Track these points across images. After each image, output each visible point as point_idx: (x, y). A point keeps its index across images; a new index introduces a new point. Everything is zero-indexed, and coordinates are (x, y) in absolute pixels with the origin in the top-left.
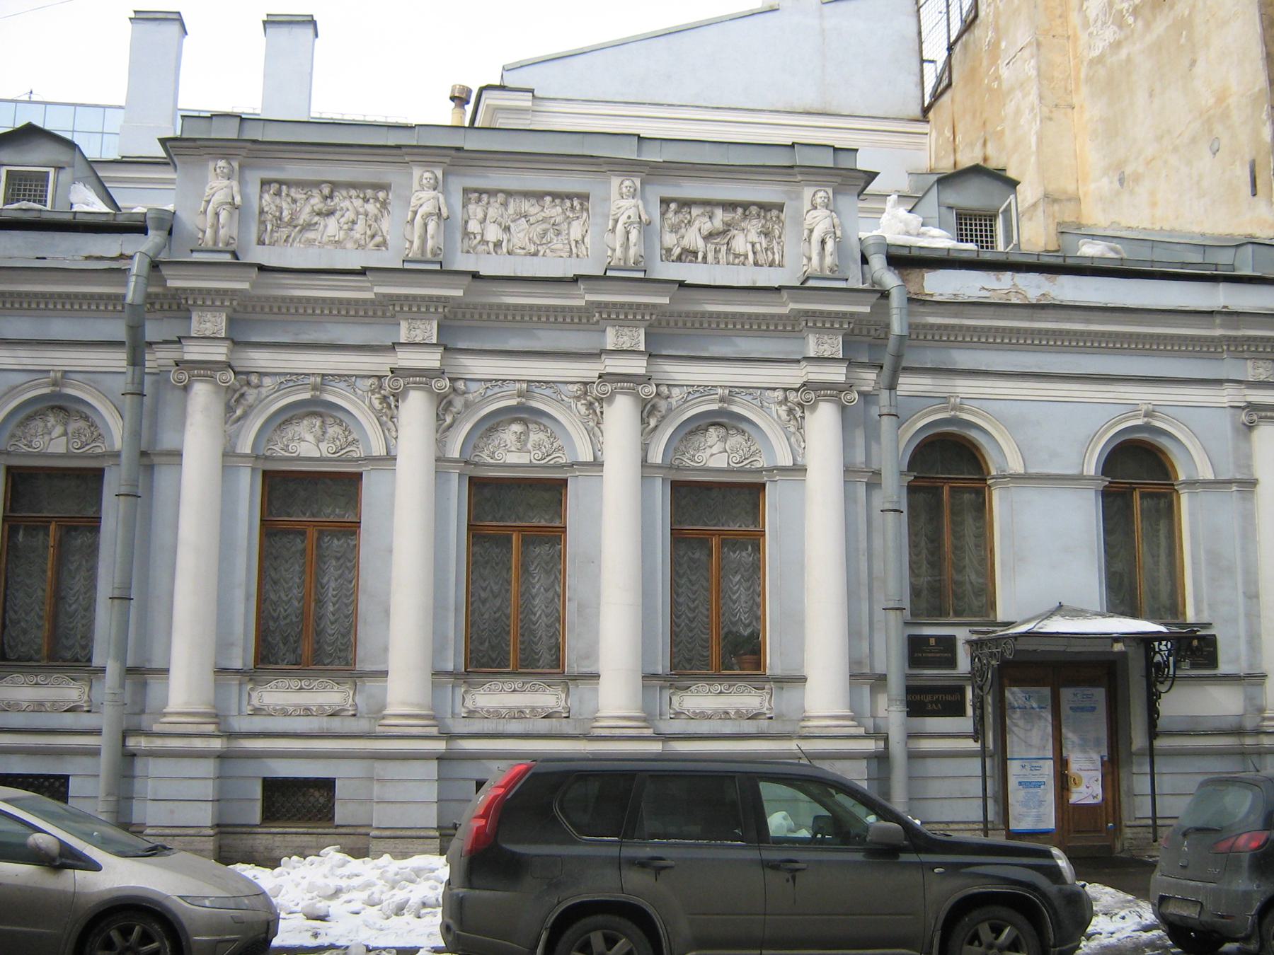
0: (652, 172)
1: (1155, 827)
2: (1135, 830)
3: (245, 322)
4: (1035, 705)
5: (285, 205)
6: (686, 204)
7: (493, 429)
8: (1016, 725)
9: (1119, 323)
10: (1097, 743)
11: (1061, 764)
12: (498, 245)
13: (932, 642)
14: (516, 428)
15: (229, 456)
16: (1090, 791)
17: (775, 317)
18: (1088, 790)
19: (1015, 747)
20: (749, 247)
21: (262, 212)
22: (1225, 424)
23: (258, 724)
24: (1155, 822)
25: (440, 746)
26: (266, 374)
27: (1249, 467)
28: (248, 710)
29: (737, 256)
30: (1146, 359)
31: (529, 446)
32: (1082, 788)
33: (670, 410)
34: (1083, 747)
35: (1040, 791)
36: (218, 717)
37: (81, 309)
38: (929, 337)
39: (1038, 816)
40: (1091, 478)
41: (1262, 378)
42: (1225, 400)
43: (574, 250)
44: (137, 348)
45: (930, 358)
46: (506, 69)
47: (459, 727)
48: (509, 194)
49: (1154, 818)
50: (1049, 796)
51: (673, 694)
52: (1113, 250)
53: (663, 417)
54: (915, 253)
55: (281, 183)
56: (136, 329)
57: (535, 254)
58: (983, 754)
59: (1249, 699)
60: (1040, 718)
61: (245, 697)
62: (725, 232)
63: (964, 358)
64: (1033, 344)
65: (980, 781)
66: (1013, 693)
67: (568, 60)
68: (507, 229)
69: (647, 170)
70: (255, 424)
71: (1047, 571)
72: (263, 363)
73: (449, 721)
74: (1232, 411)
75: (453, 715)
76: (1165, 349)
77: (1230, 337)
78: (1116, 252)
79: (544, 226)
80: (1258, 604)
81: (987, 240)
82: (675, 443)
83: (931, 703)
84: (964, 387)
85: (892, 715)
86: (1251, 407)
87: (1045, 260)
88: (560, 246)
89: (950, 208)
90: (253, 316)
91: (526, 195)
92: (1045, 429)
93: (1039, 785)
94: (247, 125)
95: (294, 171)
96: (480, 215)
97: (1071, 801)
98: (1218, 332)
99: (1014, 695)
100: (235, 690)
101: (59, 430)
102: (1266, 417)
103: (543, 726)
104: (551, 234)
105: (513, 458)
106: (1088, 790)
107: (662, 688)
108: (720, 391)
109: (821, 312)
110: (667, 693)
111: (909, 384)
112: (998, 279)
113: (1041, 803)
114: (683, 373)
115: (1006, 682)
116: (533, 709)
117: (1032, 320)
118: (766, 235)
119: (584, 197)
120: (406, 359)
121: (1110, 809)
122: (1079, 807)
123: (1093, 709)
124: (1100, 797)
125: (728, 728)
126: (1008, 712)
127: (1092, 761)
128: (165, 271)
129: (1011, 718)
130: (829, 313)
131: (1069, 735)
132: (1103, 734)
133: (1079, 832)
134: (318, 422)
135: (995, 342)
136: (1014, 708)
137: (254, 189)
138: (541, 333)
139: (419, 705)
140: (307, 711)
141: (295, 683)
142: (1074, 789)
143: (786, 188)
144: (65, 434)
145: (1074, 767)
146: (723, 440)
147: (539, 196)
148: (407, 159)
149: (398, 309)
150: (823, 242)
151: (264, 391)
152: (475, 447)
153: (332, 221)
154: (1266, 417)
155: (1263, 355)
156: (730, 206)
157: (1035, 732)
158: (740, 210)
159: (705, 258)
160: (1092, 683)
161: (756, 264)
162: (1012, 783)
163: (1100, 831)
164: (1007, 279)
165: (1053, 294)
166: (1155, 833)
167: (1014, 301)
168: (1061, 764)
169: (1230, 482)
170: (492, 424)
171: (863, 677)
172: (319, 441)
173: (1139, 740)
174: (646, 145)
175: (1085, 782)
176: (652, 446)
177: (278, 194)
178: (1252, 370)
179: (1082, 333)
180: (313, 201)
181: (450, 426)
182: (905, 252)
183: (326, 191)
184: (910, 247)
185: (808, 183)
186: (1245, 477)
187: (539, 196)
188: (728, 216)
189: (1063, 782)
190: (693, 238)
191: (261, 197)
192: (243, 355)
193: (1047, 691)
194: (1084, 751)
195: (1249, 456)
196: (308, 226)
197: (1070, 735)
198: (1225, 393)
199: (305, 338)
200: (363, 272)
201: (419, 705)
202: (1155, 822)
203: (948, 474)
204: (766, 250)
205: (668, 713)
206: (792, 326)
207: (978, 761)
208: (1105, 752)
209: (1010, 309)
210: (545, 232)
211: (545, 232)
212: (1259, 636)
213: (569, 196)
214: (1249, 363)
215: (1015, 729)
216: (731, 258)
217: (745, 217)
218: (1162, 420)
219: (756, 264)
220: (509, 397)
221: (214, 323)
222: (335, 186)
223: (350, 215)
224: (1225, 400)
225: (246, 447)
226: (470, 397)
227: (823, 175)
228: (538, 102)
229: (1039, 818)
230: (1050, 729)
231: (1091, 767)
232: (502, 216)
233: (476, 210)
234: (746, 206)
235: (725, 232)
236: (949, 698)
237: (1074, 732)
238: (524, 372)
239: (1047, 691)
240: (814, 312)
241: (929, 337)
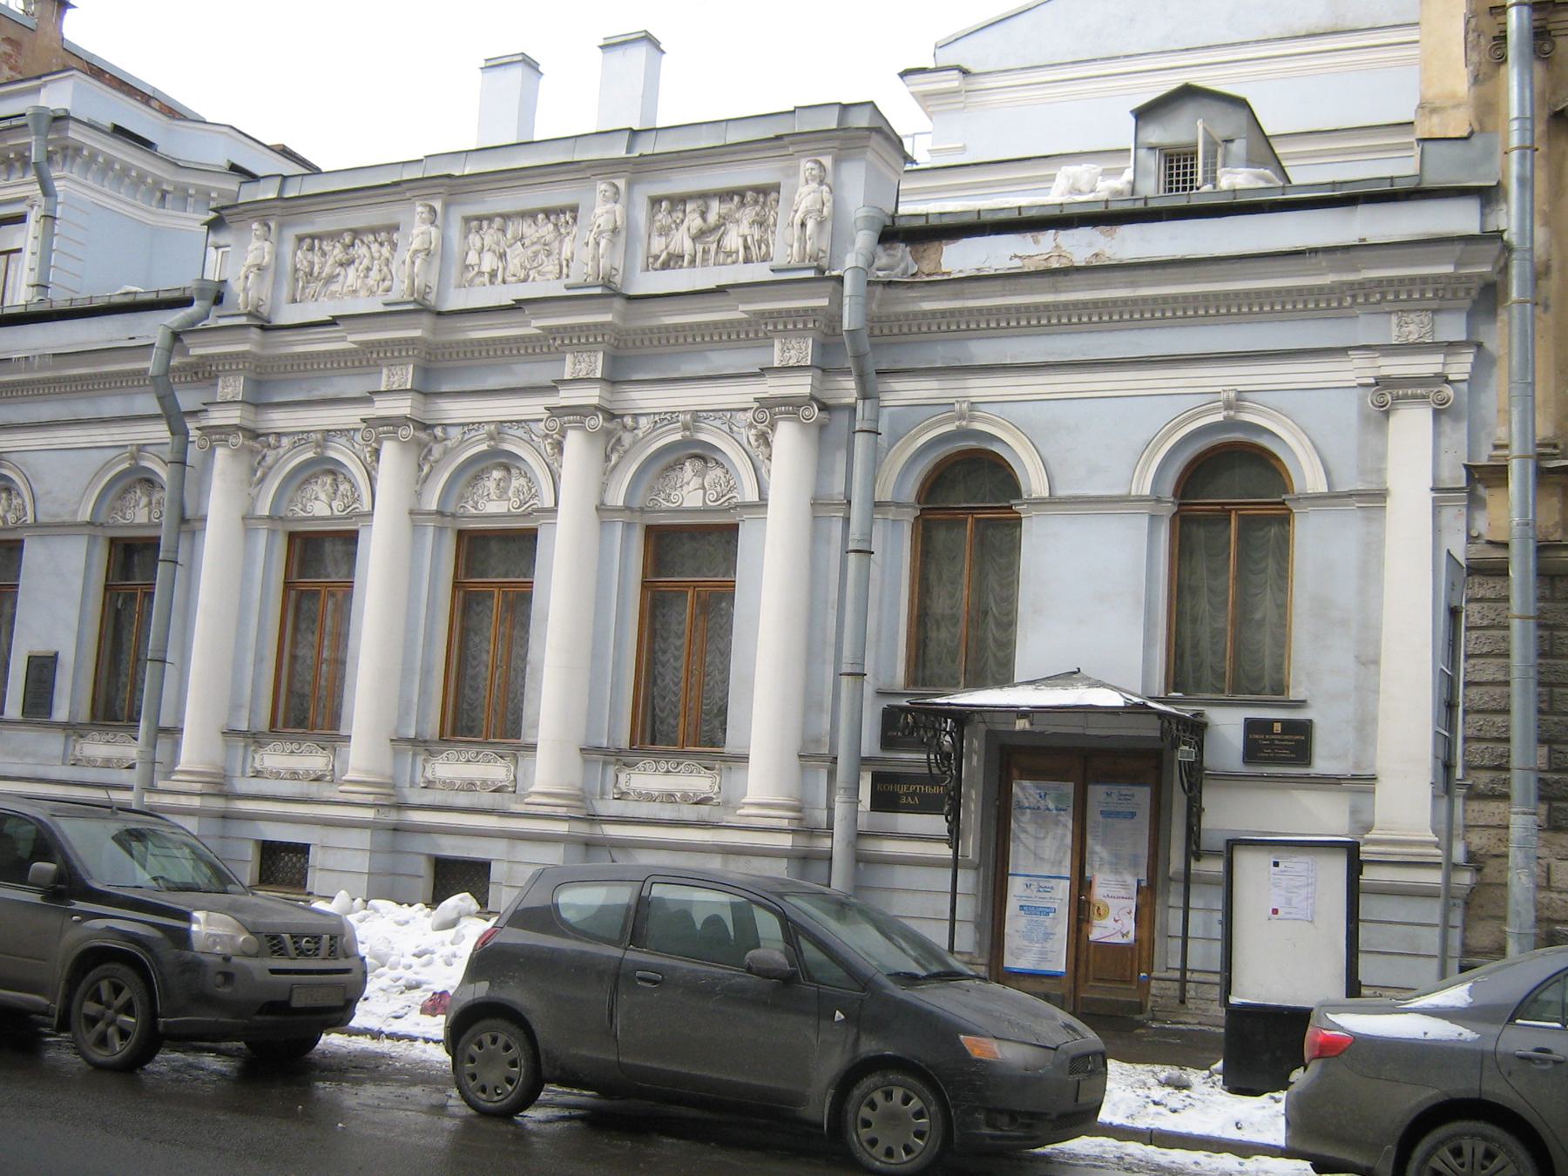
0: (638, 168)
1: (1183, 981)
2: (1163, 984)
3: (266, 384)
4: (1051, 806)
5: (316, 260)
6: (679, 201)
7: (477, 477)
8: (1025, 831)
10: (1134, 864)
11: (1081, 886)
12: (493, 275)
13: (1278, 728)
16: (1118, 926)
17: (733, 326)
19: (1019, 858)
20: (740, 241)
21: (296, 270)
22: (1349, 409)
23: (429, 797)
24: (1184, 974)
25: (582, 829)
27: (1380, 472)
28: (420, 781)
29: (729, 254)
32: (1108, 922)
35: (1047, 921)
36: (582, 797)
38: (934, 328)
39: (1042, 953)
40: (1141, 499)
41: (1412, 338)
42: (1351, 376)
43: (565, 270)
44: (175, 418)
45: (941, 355)
46: (939, 47)
47: (415, 797)
48: (506, 217)
50: (1061, 929)
51: (619, 770)
52: (1261, 177)
53: (625, 452)
54: (933, 221)
55: (313, 237)
57: (525, 281)
58: (955, 864)
59: (1354, 812)
60: (1057, 823)
61: (250, 760)
62: (717, 227)
63: (984, 351)
66: (1023, 788)
67: (1009, 22)
69: (630, 167)
70: (273, 485)
71: (1085, 626)
73: (406, 791)
74: (1360, 391)
75: (413, 784)
77: (1351, 284)
79: (535, 248)
80: (1378, 673)
81: (1188, 183)
84: (979, 388)
85: (850, 807)
86: (1382, 383)
87: (1115, 207)
88: (550, 268)
89: (1152, 148)
92: (1091, 436)
93: (1046, 912)
94: (290, 182)
95: (323, 223)
96: (478, 245)
97: (1091, 937)
98: (1328, 279)
99: (1024, 791)
100: (241, 752)
101: (144, 501)
102: (1406, 397)
103: (689, 813)
104: (542, 256)
105: (494, 507)
106: (1114, 924)
107: (605, 764)
108: (681, 417)
111: (905, 392)
112: (1036, 242)
113: (1048, 936)
115: (1015, 773)
116: (484, 782)
117: (1057, 291)
119: (574, 209)
120: (385, 407)
124: (1131, 937)
125: (667, 812)
127: (1125, 886)
128: (187, 340)
131: (1096, 848)
133: (1099, 980)
134: (329, 480)
136: (1021, 807)
137: (288, 247)
138: (519, 368)
140: (294, 775)
141: (289, 747)
144: (150, 503)
146: (701, 474)
148: (408, 195)
150: (803, 225)
152: (462, 497)
153: (351, 270)
154: (1406, 397)
155: (1425, 305)
156: (725, 195)
157: (1048, 842)
158: (736, 199)
159: (693, 262)
160: (1135, 779)
162: (1012, 905)
163: (1130, 982)
164: (1048, 238)
165: (1108, 253)
166: (1183, 990)
167: (1055, 265)
168: (1081, 886)
169: (1349, 495)
171: (812, 756)
172: (332, 499)
177: (311, 249)
178: (1393, 330)
180: (336, 251)
182: (921, 222)
183: (348, 240)
184: (927, 215)
186: (1373, 487)
187: (531, 215)
188: (725, 208)
189: (1082, 910)
190: (682, 241)
191: (295, 254)
192: (266, 417)
193: (1069, 788)
194: (1116, 872)
195: (1382, 456)
196: (331, 279)
197: (1098, 848)
198: (1348, 366)
199: (329, 392)
200: (333, 322)
202: (1184, 974)
203: (969, 503)
204: (759, 243)
205: (611, 792)
206: (756, 331)
207: (949, 873)
208: (1143, 876)
209: (1023, 281)
210: (536, 254)
211: (536, 254)
212: (1375, 720)
213: (560, 211)
214: (1394, 319)
215: (1022, 836)
216: (722, 256)
217: (742, 204)
219: (504, 282)
220: (481, 441)
221: (232, 387)
222: (356, 233)
223: (366, 262)
224: (1351, 376)
225: (264, 509)
226: (449, 443)
227: (816, 141)
228: (971, 79)
229: (1043, 956)
230: (1069, 840)
231: (1123, 893)
232: (498, 244)
233: (474, 239)
234: (740, 193)
235: (717, 227)
236: (929, 790)
237: (1104, 843)
239: (1069, 788)
241: (934, 328)
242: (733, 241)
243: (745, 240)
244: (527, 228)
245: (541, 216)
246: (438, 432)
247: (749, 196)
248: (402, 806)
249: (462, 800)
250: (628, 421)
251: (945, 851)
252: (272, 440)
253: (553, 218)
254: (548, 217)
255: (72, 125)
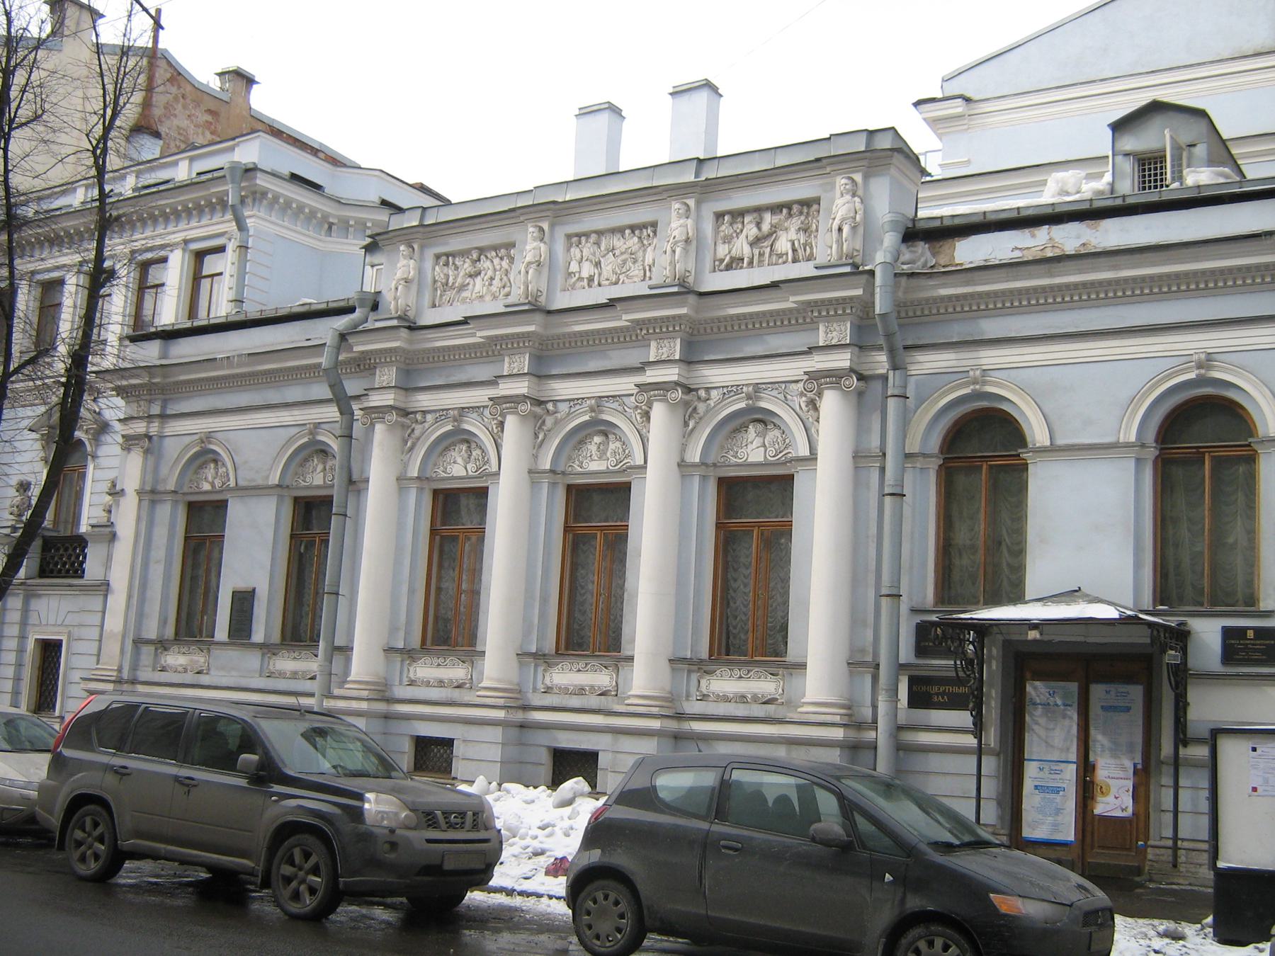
0: (705, 189)
1: (1175, 848)
2: (1157, 851)
4: (1059, 702)
7: (582, 442)
8: (1037, 723)
9: (1081, 272)
11: (1086, 768)
12: (591, 279)
13: (1250, 634)
14: (597, 439)
15: (402, 479)
16: (1118, 802)
18: (1115, 800)
20: (789, 245)
21: (435, 281)
23: (549, 700)
26: (429, 412)
28: (541, 687)
29: (780, 256)
30: (1211, 300)
31: (608, 454)
33: (708, 411)
34: (1114, 753)
35: (1058, 798)
37: (1225, 286)
40: (1128, 445)
44: (343, 401)
45: (957, 331)
47: (537, 700)
48: (600, 233)
49: (1175, 838)
54: (947, 223)
55: (447, 255)
56: (337, 387)
57: (616, 283)
58: (979, 752)
60: (1064, 716)
62: (770, 235)
63: (992, 327)
64: (1029, 305)
65: (974, 779)
66: (1035, 688)
68: (598, 264)
69: (698, 189)
72: (425, 404)
73: (530, 695)
76: (1244, 284)
78: (1227, 177)
79: (624, 257)
82: (720, 438)
83: (937, 694)
84: (990, 358)
90: (558, 352)
91: (613, 231)
93: (1057, 790)
94: (428, 212)
95: (455, 244)
96: (579, 256)
97: (1096, 812)
99: (1036, 690)
101: (320, 467)
103: (758, 710)
104: (629, 263)
105: (595, 466)
106: (1115, 800)
107: (690, 672)
109: (823, 301)
110: (694, 677)
111: (927, 363)
112: (1033, 236)
113: (1058, 811)
114: (565, 389)
115: (1028, 675)
116: (592, 687)
117: (1052, 276)
118: (805, 231)
119: (654, 225)
120: (506, 389)
121: (1142, 825)
122: (1107, 820)
123: (1128, 709)
124: (1130, 810)
125: (741, 711)
126: (1029, 708)
127: (1124, 769)
128: (351, 340)
129: (1031, 715)
130: (830, 301)
132: (1138, 739)
133: (1103, 847)
134: (464, 447)
135: (1055, 302)
136: (1035, 704)
138: (611, 353)
139: (499, 680)
140: (441, 684)
142: (1100, 798)
143: (821, 182)
145: (1101, 774)
146: (762, 435)
147: (620, 230)
149: (816, 314)
151: (712, 403)
156: (776, 208)
158: (785, 211)
160: (1129, 679)
161: (600, 285)
163: (1129, 849)
165: (1094, 242)
166: (1175, 856)
168: (1086, 768)
170: (579, 437)
171: (859, 663)
173: (1167, 748)
174: (707, 165)
175: (1113, 791)
176: (690, 447)
177: (447, 264)
179: (1109, 282)
180: (466, 265)
181: (692, 430)
182: (937, 224)
183: (475, 256)
184: (942, 218)
185: (837, 172)
187: (620, 230)
188: (776, 219)
189: (1087, 789)
190: (742, 247)
191: (434, 269)
193: (1074, 687)
196: (463, 287)
197: (1100, 737)
200: (465, 321)
201: (499, 680)
203: (983, 454)
204: (805, 245)
206: (805, 317)
208: (1138, 759)
210: (624, 262)
211: (624, 262)
213: (643, 226)
215: (1035, 727)
217: (790, 215)
218: (1225, 370)
219: (600, 285)
221: (387, 376)
223: (490, 273)
226: (559, 415)
229: (1056, 827)
231: (1122, 774)
232: (594, 254)
234: (788, 206)
236: (956, 690)
237: (1104, 734)
238: (594, 389)
239: (1074, 687)
240: (816, 302)
242: (783, 245)
243: (793, 244)
244: (617, 242)
245: (627, 232)
246: (550, 406)
247: (795, 208)
248: (526, 708)
249: (575, 702)
250: (702, 393)
251: (971, 741)
252: (419, 417)
253: (637, 232)
254: (633, 232)
255: (259, 175)
